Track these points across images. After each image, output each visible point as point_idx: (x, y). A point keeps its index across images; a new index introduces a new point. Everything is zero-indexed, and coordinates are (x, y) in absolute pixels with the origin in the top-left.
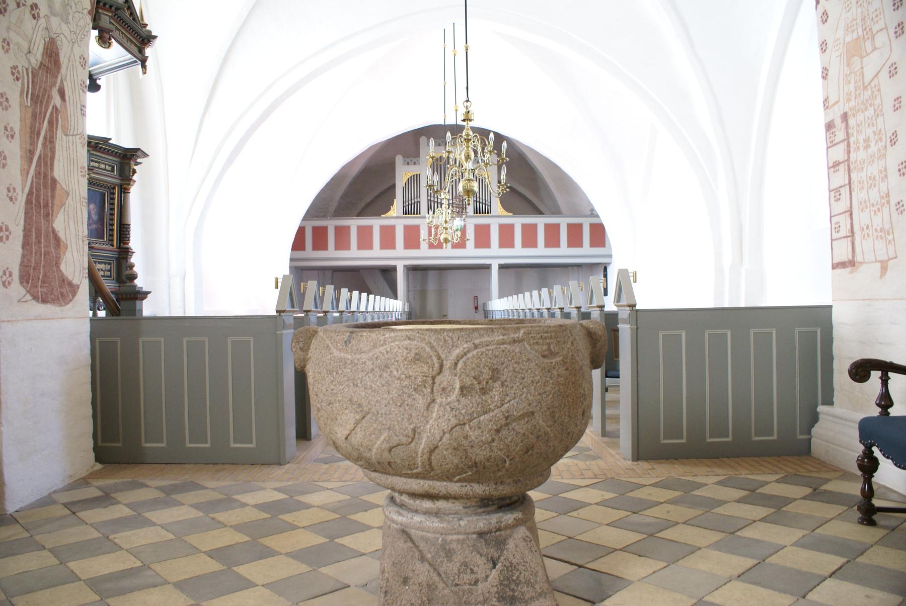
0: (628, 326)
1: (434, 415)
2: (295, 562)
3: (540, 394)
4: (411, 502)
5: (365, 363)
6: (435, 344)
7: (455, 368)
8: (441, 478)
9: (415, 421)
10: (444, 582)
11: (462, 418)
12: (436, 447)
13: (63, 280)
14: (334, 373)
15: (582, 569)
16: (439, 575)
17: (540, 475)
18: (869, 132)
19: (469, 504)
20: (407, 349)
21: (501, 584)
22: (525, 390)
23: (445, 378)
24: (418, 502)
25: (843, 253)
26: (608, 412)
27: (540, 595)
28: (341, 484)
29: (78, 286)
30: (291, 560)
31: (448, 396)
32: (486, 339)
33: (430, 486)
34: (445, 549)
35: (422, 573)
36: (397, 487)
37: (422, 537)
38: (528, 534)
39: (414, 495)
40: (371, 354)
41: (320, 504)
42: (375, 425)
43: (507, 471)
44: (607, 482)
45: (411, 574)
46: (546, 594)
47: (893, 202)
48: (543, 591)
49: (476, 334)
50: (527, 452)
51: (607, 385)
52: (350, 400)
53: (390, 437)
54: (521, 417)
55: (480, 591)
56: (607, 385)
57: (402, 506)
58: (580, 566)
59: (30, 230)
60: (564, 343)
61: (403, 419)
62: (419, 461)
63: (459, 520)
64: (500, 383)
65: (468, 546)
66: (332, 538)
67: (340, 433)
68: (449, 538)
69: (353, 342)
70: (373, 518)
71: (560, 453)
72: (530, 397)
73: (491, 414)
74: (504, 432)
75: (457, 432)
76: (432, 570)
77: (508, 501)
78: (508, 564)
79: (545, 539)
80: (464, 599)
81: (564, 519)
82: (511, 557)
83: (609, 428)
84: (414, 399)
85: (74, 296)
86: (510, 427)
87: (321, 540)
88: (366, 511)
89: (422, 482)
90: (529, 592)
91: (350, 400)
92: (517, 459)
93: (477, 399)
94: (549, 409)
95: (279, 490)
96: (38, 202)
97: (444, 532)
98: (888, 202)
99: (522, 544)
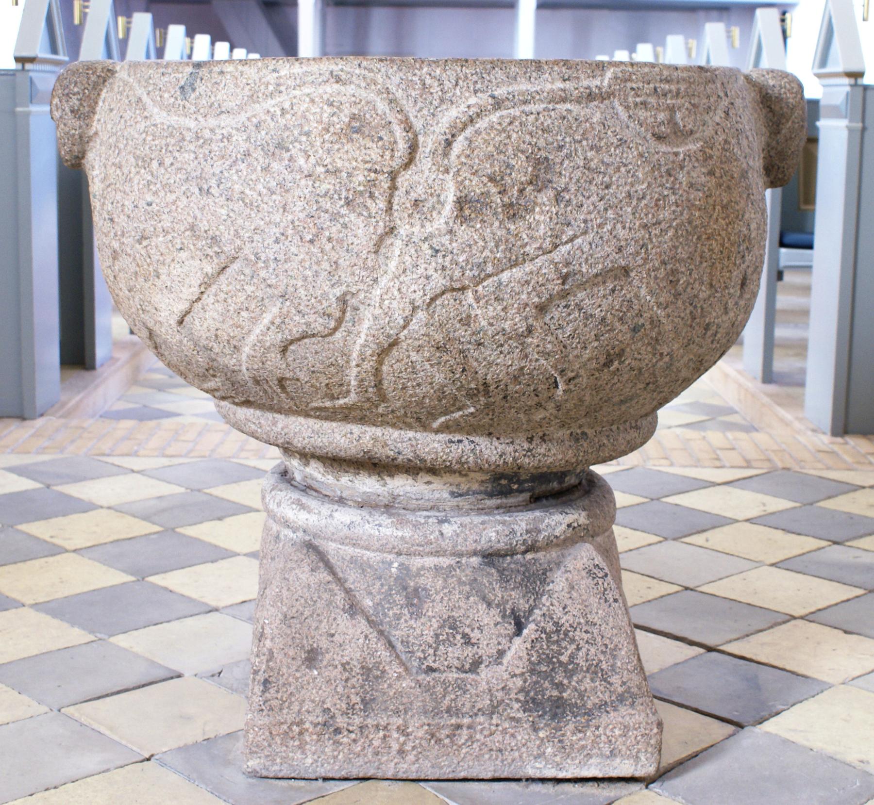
0: (843, 123)
1: (393, 265)
2: (56, 622)
3: (645, 226)
4: (330, 479)
5: (229, 138)
6: (399, 94)
7: (446, 155)
8: (401, 421)
9: (346, 277)
10: (402, 664)
11: (457, 274)
12: (394, 344)
14: (155, 164)
15: (714, 655)
16: (391, 646)
17: (637, 429)
19: (464, 488)
20: (331, 105)
21: (532, 671)
22: (610, 214)
23: (419, 178)
24: (345, 479)
26: (780, 332)
27: (621, 699)
28: (165, 461)
30: (48, 618)
31: (427, 218)
32: (523, 86)
33: (375, 439)
34: (405, 588)
35: (351, 639)
36: (298, 443)
37: (353, 560)
38: (599, 560)
39: (336, 462)
40: (243, 117)
41: (113, 502)
42: (249, 289)
43: (558, 408)
44: (773, 476)
45: (324, 643)
46: (634, 696)
48: (628, 691)
49: (499, 74)
50: (608, 364)
51: (783, 263)
52: (192, 228)
53: (284, 317)
54: (601, 277)
55: (483, 686)
56: (783, 263)
57: (307, 489)
58: (710, 649)
60: (708, 110)
61: (316, 274)
62: (352, 376)
63: (441, 522)
64: (551, 193)
65: (460, 582)
66: (141, 574)
67: (167, 308)
68: (416, 562)
69: (201, 88)
70: (240, 534)
71: (684, 373)
72: (622, 233)
73: (528, 267)
74: (556, 313)
75: (446, 306)
76: (373, 635)
77: (555, 485)
78: (550, 627)
79: (635, 588)
80: (446, 702)
81: (672, 548)
82: (558, 612)
83: (780, 364)
84: (345, 226)
86: (572, 301)
87: (116, 578)
88: (220, 519)
89: (356, 429)
90: (594, 692)
91: (192, 228)
92: (584, 381)
93: (495, 228)
94: (664, 263)
95: (20, 471)
97: (404, 547)
99: (586, 583)
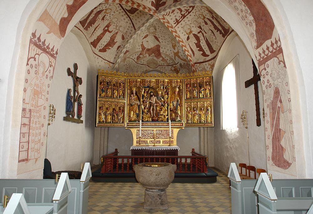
13: (285, 161)
18: (37, 120)
25: (24, 156)
29: (291, 164)
47: (41, 142)
59: (274, 146)
85: (289, 167)
96: (276, 137)
98: (40, 142)
